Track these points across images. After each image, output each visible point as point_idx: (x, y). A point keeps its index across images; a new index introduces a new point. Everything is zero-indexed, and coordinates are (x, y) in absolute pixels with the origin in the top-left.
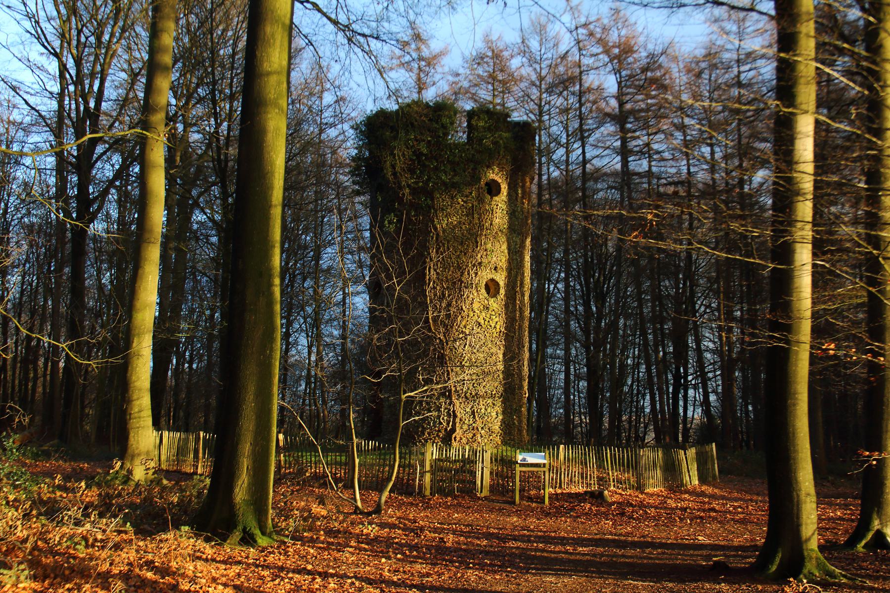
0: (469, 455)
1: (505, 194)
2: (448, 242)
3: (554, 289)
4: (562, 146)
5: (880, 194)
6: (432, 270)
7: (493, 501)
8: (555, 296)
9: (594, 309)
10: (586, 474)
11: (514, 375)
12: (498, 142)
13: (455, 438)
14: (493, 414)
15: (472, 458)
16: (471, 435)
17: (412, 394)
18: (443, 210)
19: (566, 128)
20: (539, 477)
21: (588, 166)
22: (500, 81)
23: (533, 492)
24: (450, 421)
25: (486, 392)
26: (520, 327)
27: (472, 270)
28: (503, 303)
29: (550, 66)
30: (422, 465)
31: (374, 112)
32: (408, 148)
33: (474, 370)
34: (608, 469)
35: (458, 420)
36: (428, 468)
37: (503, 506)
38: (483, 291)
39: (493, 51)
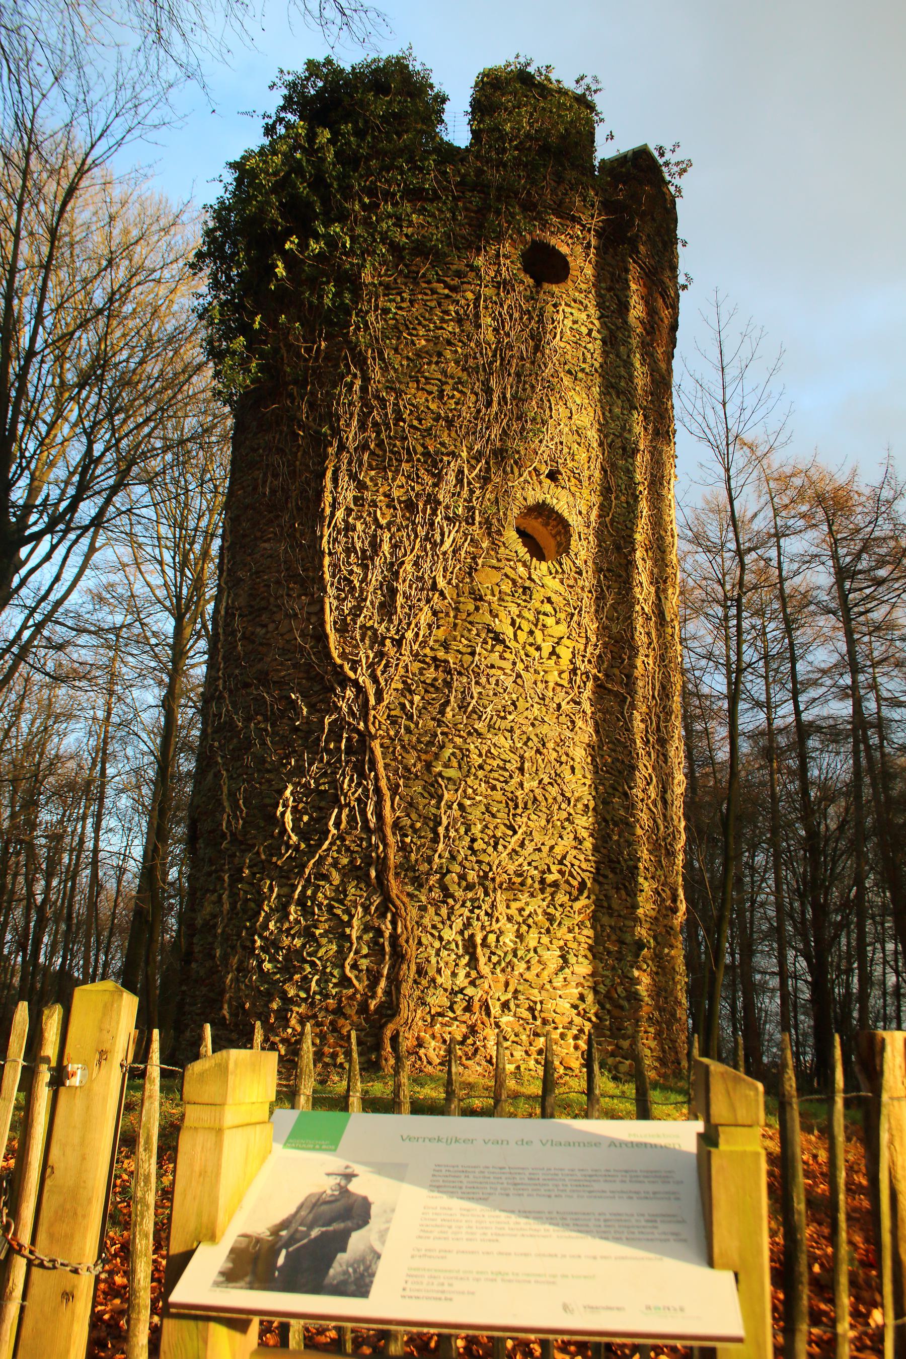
6: (344, 480)
13: (395, 1039)
14: (546, 955)
35: (409, 972)
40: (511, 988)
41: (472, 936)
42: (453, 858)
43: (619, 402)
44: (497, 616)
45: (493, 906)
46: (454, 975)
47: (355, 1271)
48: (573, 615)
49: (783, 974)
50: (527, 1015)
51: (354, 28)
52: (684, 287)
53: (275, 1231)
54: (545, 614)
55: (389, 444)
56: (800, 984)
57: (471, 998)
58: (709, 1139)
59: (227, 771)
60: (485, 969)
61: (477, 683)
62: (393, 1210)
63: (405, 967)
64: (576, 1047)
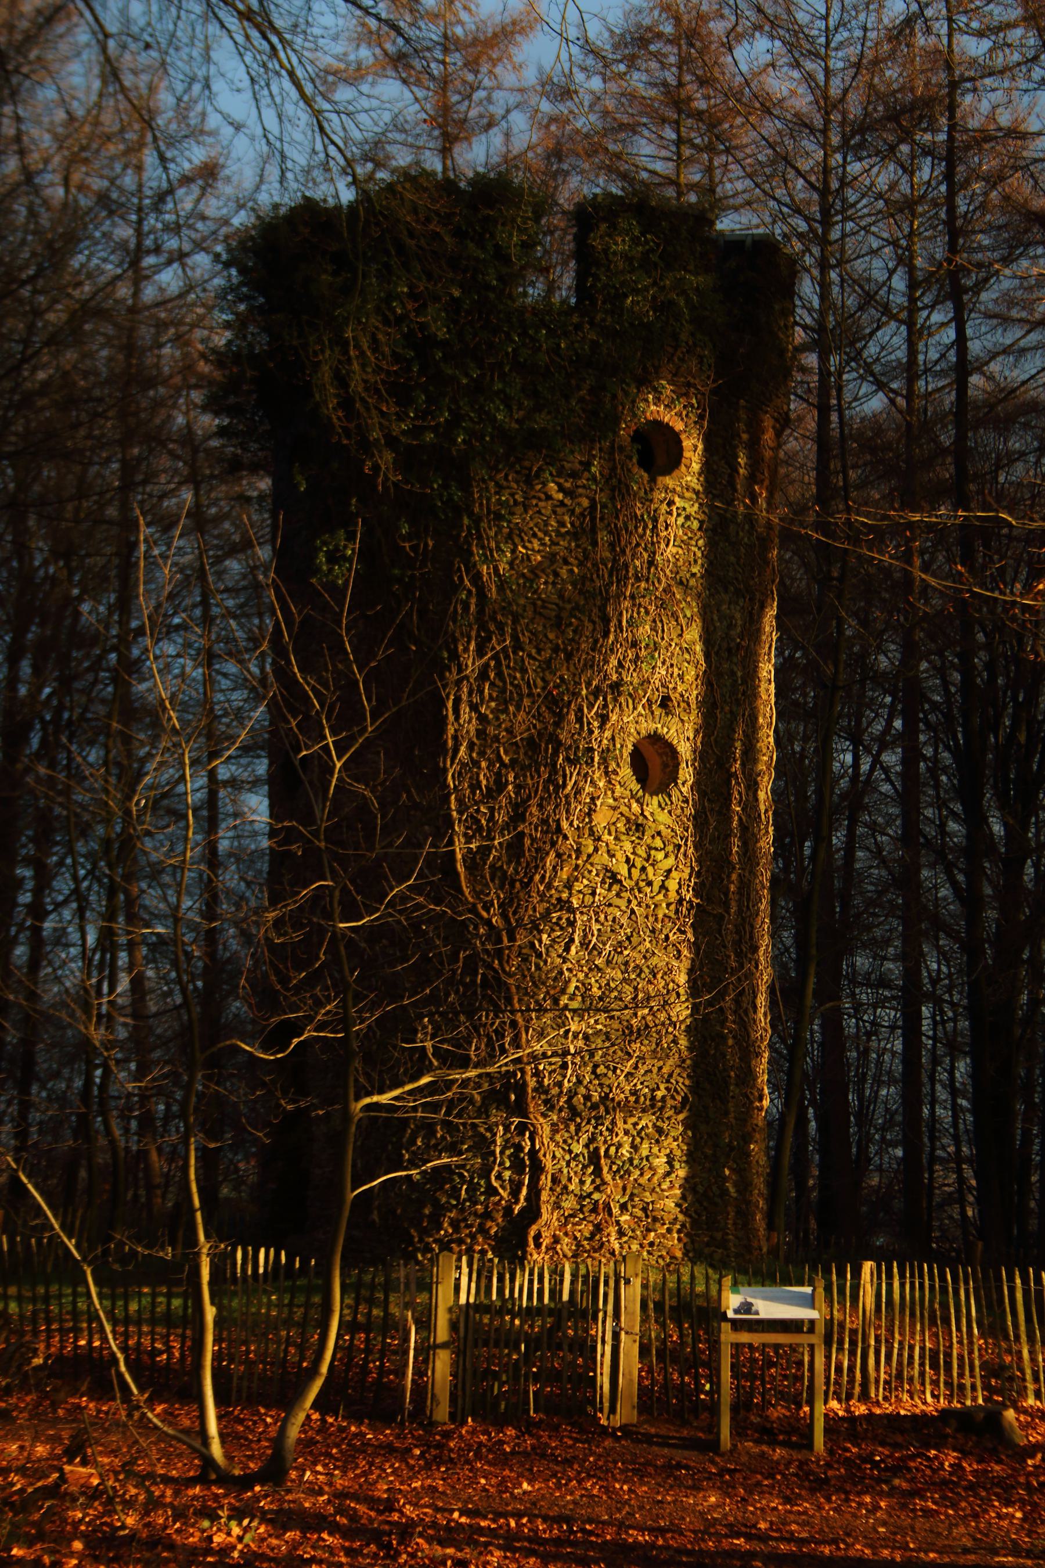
0: (572, 1293)
1: (696, 467)
2: (516, 621)
3: (872, 769)
4: (894, 317)
5: (87, 327)
6: (465, 709)
7: (648, 1439)
8: (876, 790)
9: (997, 828)
10: (948, 1355)
11: (724, 1038)
12: (672, 303)
13: (538, 1237)
14: (656, 1162)
15: (585, 1303)
16: (586, 1229)
17: (384, 1098)
18: (499, 517)
19: (905, 260)
20: (800, 1363)
21: (975, 379)
22: (699, 115)
23: (778, 1412)
24: (520, 1184)
25: (634, 1093)
26: (746, 887)
27: (591, 706)
28: (690, 810)
29: (858, 65)
30: (425, 1323)
31: (283, 211)
32: (386, 322)
33: (598, 1022)
34: (1017, 1337)
35: (546, 1181)
36: (442, 1333)
37: (679, 1455)
38: (626, 772)
39: (678, 20)
40: (628, 1192)
41: (597, 1149)
42: (579, 1082)
44: (613, 856)
45: (613, 1123)
46: (582, 1182)
48: (680, 846)
50: (640, 1214)
54: (656, 849)
55: (509, 675)
57: (597, 1201)
58: (814, 1291)
60: (608, 1177)
61: (597, 921)
63: (543, 1177)
64: (679, 1240)
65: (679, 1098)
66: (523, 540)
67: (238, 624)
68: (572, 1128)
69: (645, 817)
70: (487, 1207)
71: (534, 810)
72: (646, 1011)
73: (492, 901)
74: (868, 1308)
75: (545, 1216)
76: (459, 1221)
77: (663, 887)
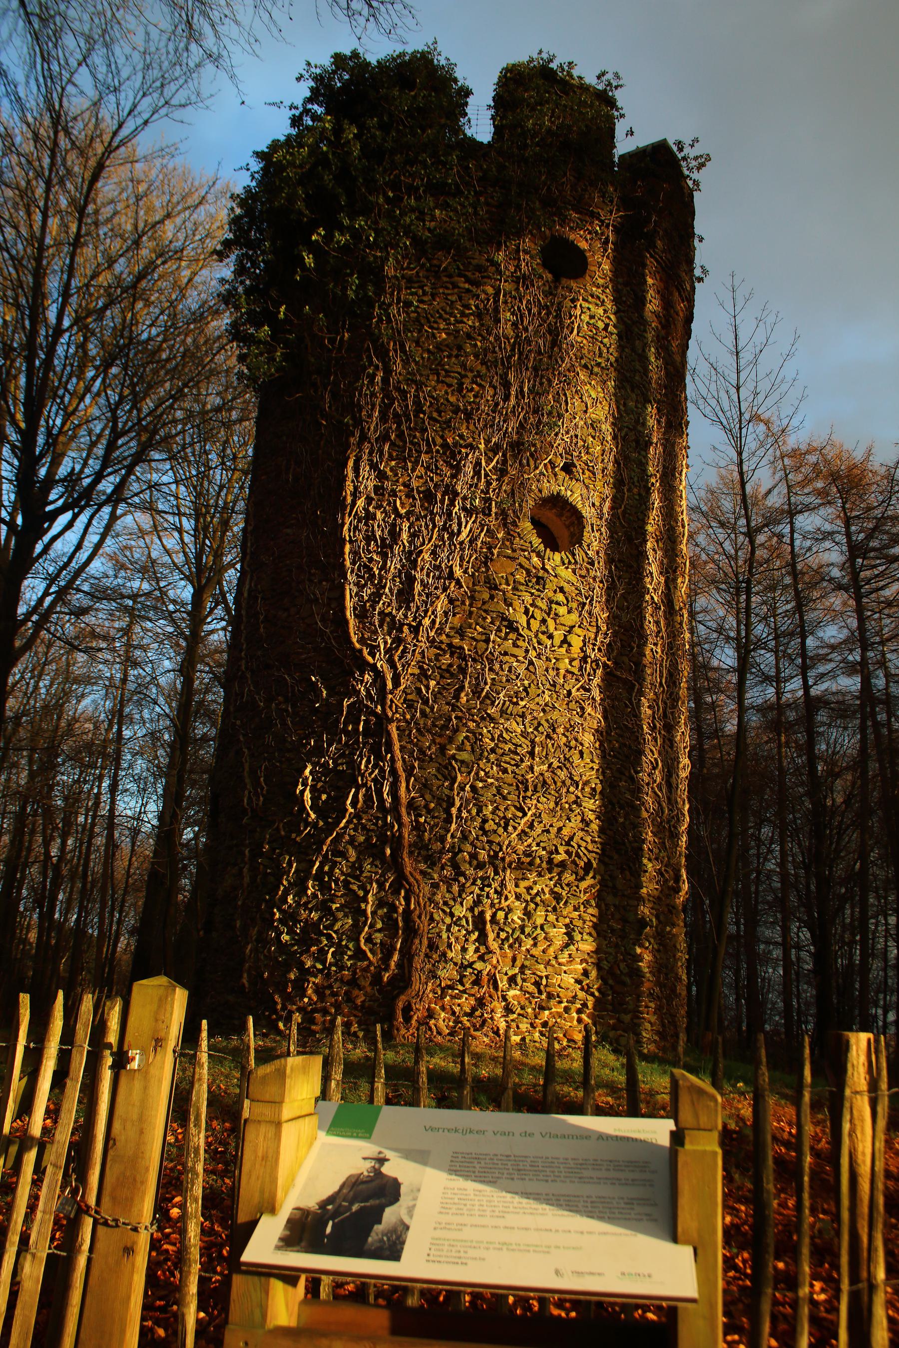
13: (407, 1011)
14: (553, 932)
16: (466, 1003)
27: (489, 460)
35: (421, 946)
41: (482, 913)
42: (465, 837)
43: (634, 396)
44: (511, 605)
45: (503, 884)
46: (464, 950)
47: (389, 1239)
48: (584, 604)
49: (786, 946)
50: (532, 988)
51: (381, 20)
52: (700, 280)
53: (323, 1205)
54: (558, 603)
55: (409, 435)
56: (803, 954)
57: (480, 972)
58: (677, 1137)
59: (249, 749)
60: (494, 945)
62: (419, 1190)
63: (417, 941)
65: (582, 864)
66: (429, 322)
67: (146, 395)
68: (455, 888)
69: (546, 571)
70: (355, 973)
71: (426, 556)
72: (545, 767)
73: (379, 646)
74: (865, 1169)
75: (416, 986)
76: (325, 988)
77: (565, 641)
